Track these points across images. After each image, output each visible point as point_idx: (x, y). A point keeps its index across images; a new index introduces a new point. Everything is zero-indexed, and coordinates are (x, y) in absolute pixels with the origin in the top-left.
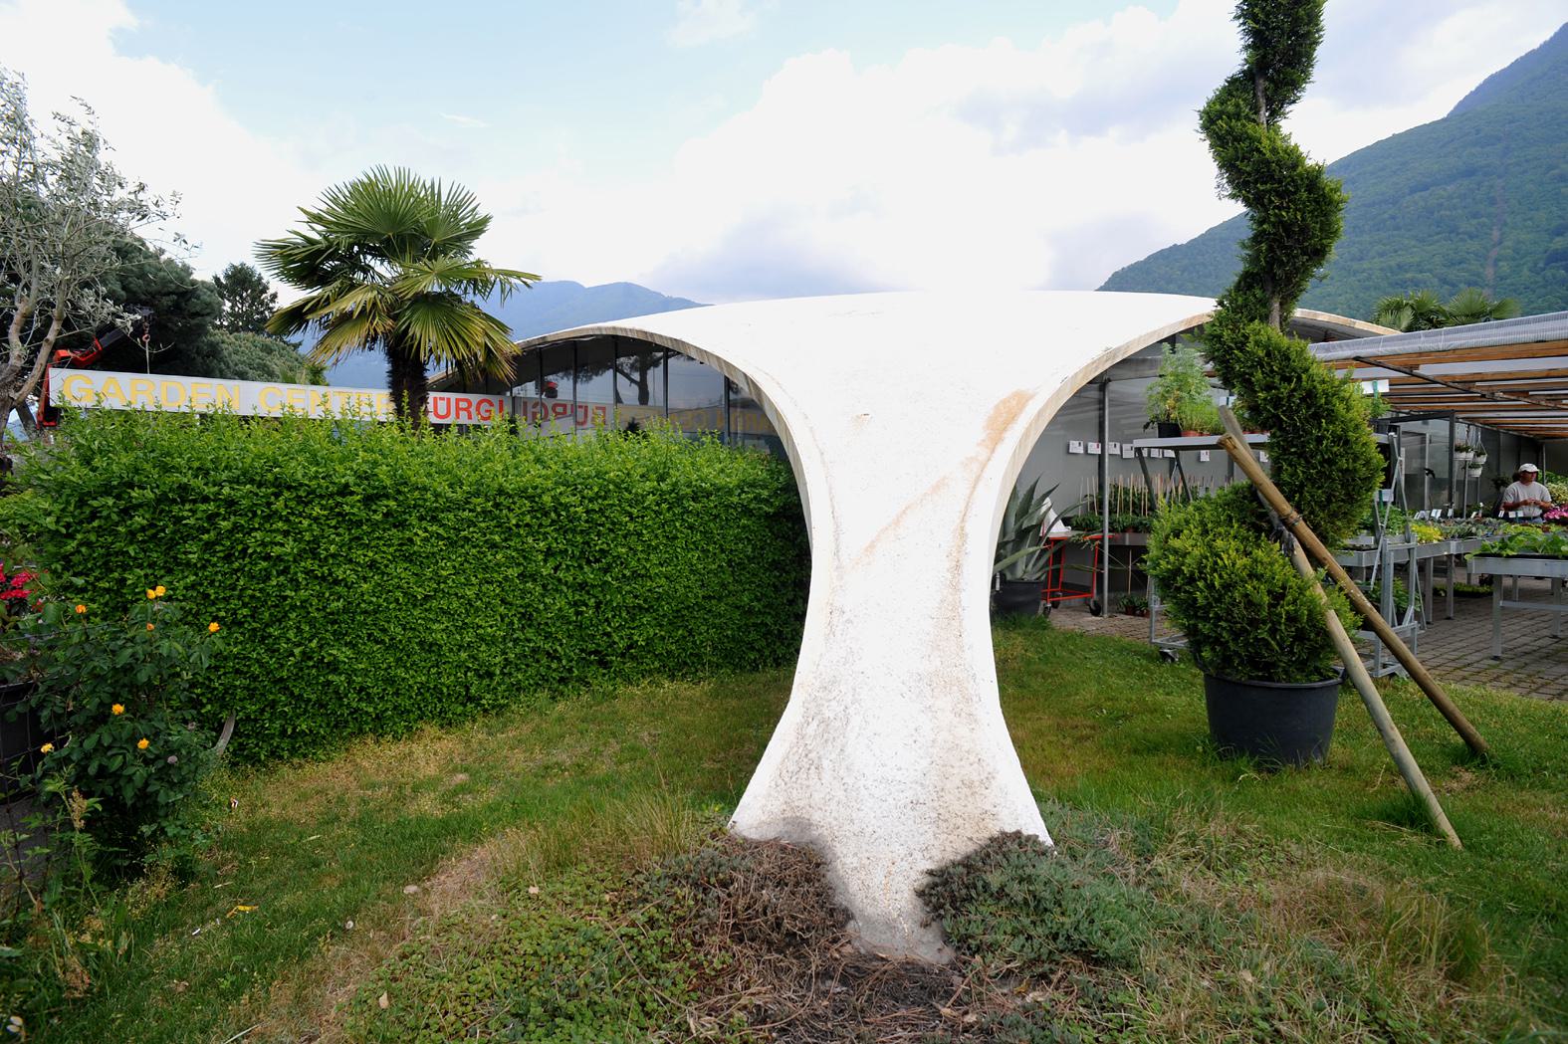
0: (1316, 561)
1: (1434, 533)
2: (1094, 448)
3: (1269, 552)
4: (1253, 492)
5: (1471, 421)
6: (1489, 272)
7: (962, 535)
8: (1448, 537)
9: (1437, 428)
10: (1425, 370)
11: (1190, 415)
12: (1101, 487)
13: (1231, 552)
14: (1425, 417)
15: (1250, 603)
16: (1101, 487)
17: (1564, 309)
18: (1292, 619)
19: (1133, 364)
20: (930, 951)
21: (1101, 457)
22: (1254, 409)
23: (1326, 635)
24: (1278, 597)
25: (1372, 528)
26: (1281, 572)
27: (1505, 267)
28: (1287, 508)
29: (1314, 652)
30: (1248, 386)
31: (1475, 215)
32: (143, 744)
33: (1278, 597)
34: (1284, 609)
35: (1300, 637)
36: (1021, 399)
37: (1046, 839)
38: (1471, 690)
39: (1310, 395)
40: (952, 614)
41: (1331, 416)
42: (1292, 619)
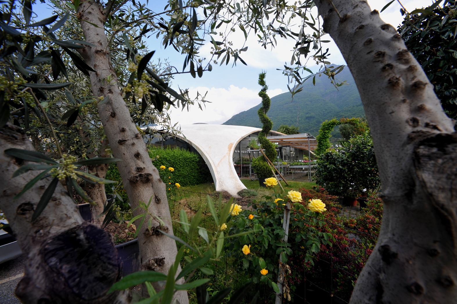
0: (271, 164)
1: (286, 163)
2: (239, 152)
3: (265, 163)
4: (263, 156)
5: (293, 147)
6: (298, 120)
7: (230, 163)
8: (288, 164)
9: (288, 148)
10: (284, 140)
11: (254, 147)
12: (240, 157)
13: (261, 163)
14: (286, 146)
15: (264, 169)
16: (240, 157)
17: (2, 284)
18: (268, 170)
19: (245, 139)
20: (239, 197)
21: (240, 153)
22: (264, 147)
23: (272, 172)
24: (267, 168)
25: (277, 161)
26: (267, 165)
27: (300, 119)
28: (267, 158)
29: (271, 174)
30: (263, 143)
31: (295, 109)
32: (169, 177)
33: (267, 168)
34: (268, 169)
35: (269, 172)
36: (232, 144)
37: (246, 188)
38: (289, 181)
39: (269, 145)
40: (231, 171)
41: (272, 147)
42: (268, 170)
